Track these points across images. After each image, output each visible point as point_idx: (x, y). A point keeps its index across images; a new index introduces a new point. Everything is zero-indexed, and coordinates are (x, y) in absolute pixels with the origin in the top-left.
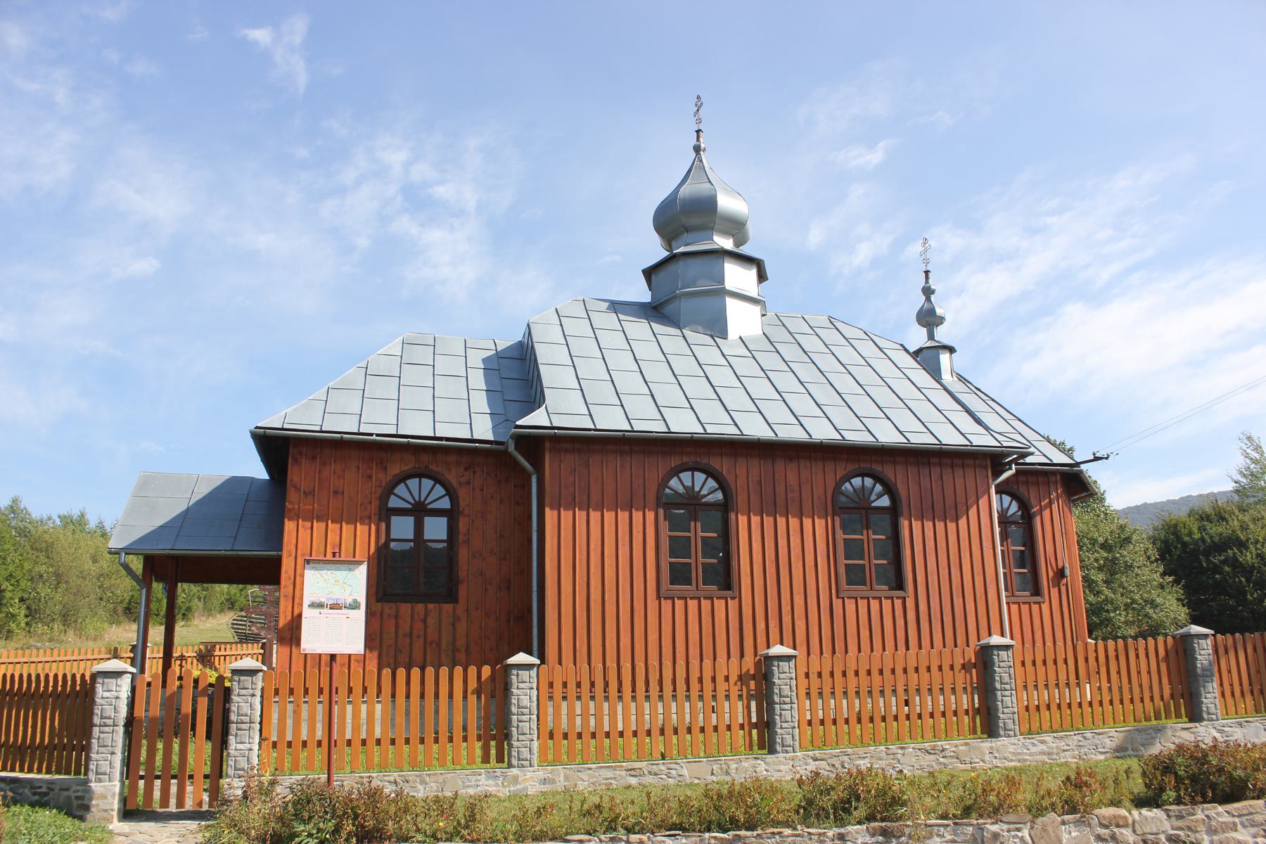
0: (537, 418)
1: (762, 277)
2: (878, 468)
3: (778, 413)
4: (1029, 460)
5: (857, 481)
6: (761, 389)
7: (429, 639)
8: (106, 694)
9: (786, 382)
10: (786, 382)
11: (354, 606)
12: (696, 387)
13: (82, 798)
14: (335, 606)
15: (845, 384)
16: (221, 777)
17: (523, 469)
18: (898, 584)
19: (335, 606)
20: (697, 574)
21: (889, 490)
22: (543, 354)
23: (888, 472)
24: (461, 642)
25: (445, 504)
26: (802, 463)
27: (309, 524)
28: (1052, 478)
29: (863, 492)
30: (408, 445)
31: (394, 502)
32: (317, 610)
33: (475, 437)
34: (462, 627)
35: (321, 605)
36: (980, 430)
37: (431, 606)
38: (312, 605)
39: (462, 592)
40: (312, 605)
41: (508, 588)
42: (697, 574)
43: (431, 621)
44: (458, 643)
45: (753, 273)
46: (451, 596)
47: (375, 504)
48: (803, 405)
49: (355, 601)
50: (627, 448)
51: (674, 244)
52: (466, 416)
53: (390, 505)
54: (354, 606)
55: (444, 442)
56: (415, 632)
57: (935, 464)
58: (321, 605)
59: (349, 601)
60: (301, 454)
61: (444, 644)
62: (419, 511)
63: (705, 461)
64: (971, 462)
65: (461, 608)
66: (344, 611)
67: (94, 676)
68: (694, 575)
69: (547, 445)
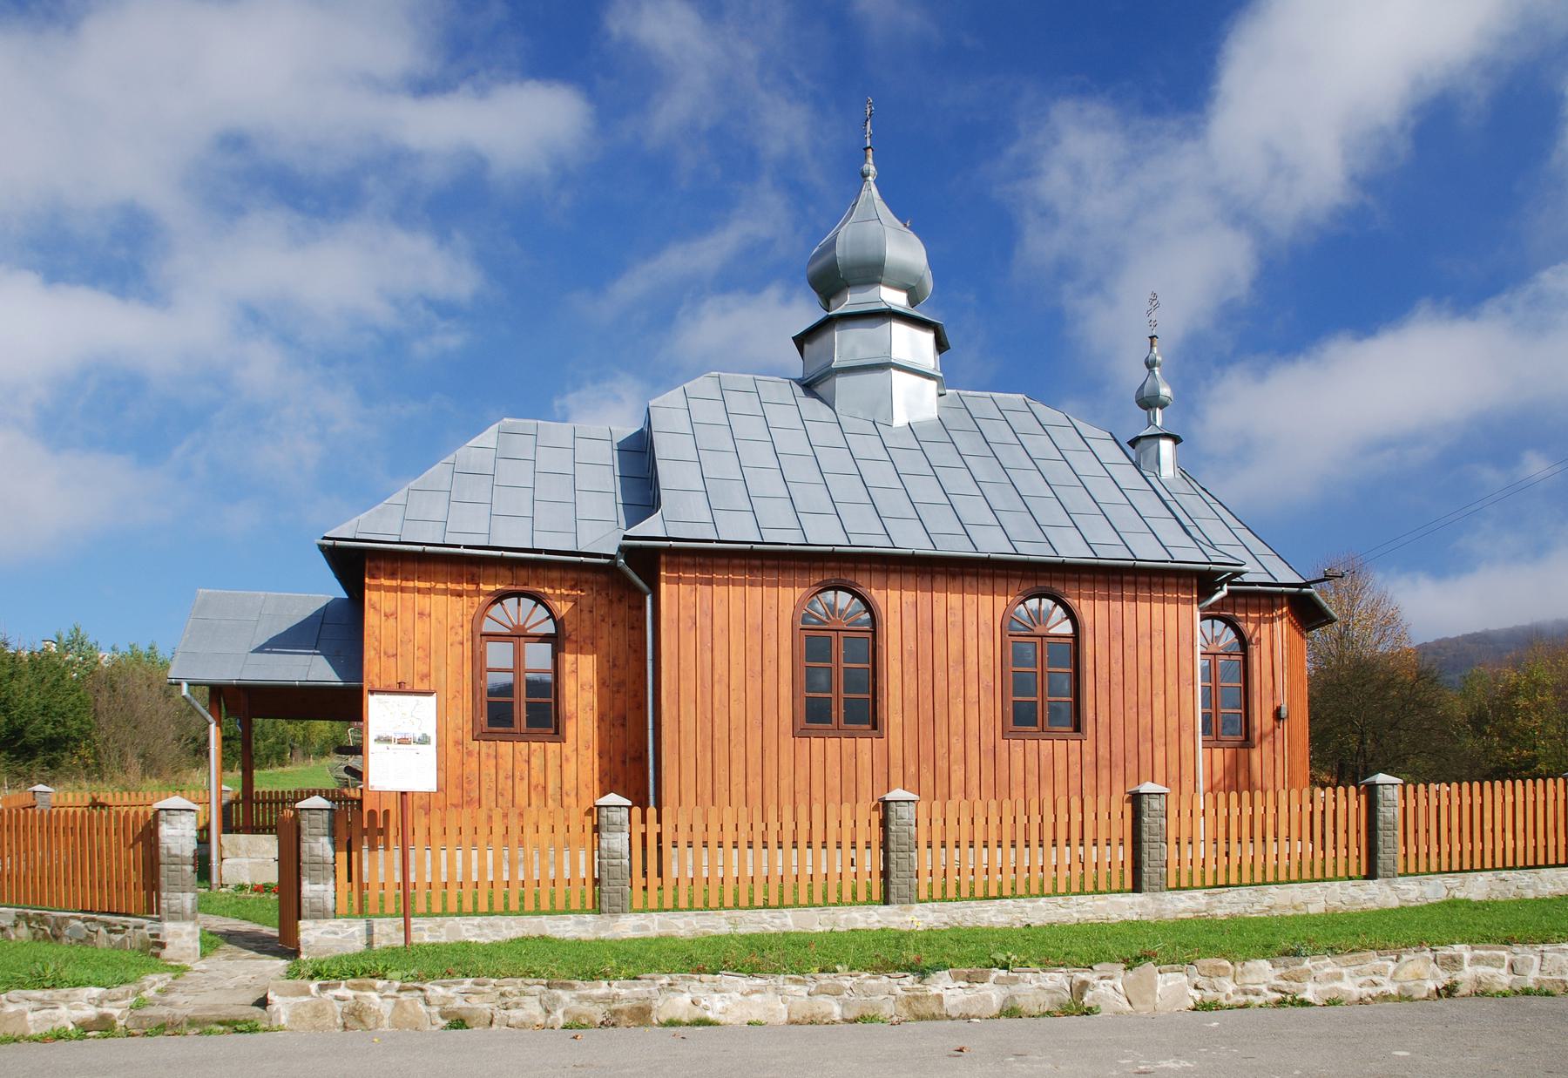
0: (651, 527)
1: (941, 345)
2: (1058, 587)
3: (1018, 525)
4: (1246, 578)
5: (1033, 603)
6: (925, 490)
7: (534, 782)
8: (172, 832)
9: (958, 481)
10: (958, 481)
11: (424, 741)
12: (845, 488)
13: (157, 936)
14: (403, 741)
15: (1030, 483)
16: (299, 918)
17: (637, 589)
18: (1078, 727)
19: (403, 741)
20: (837, 712)
21: (1071, 614)
22: (663, 447)
23: (862, 580)
24: (569, 785)
25: (549, 627)
26: (968, 579)
27: (1349, 802)
28: (1278, 601)
29: (1039, 617)
30: (502, 557)
31: (488, 626)
32: (385, 745)
33: (582, 549)
34: (570, 769)
35: (388, 740)
36: (1188, 541)
37: (534, 745)
38: (379, 740)
39: (570, 729)
40: (379, 740)
41: (623, 725)
42: (837, 712)
43: (536, 762)
44: (566, 787)
45: (928, 338)
46: (558, 734)
47: (468, 627)
48: (1049, 512)
49: (425, 735)
50: (757, 563)
51: (833, 302)
52: (599, 529)
53: (485, 629)
54: (424, 741)
55: (543, 556)
56: (517, 774)
57: (1129, 583)
58: (388, 740)
59: (418, 735)
60: (378, 568)
61: (550, 791)
62: (518, 635)
63: (850, 578)
64: (1173, 580)
65: (568, 748)
66: (413, 746)
67: (157, 813)
68: (834, 713)
69: (663, 559)
